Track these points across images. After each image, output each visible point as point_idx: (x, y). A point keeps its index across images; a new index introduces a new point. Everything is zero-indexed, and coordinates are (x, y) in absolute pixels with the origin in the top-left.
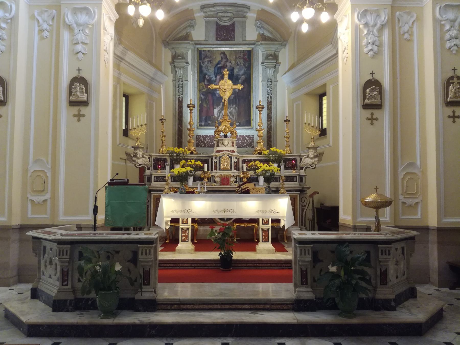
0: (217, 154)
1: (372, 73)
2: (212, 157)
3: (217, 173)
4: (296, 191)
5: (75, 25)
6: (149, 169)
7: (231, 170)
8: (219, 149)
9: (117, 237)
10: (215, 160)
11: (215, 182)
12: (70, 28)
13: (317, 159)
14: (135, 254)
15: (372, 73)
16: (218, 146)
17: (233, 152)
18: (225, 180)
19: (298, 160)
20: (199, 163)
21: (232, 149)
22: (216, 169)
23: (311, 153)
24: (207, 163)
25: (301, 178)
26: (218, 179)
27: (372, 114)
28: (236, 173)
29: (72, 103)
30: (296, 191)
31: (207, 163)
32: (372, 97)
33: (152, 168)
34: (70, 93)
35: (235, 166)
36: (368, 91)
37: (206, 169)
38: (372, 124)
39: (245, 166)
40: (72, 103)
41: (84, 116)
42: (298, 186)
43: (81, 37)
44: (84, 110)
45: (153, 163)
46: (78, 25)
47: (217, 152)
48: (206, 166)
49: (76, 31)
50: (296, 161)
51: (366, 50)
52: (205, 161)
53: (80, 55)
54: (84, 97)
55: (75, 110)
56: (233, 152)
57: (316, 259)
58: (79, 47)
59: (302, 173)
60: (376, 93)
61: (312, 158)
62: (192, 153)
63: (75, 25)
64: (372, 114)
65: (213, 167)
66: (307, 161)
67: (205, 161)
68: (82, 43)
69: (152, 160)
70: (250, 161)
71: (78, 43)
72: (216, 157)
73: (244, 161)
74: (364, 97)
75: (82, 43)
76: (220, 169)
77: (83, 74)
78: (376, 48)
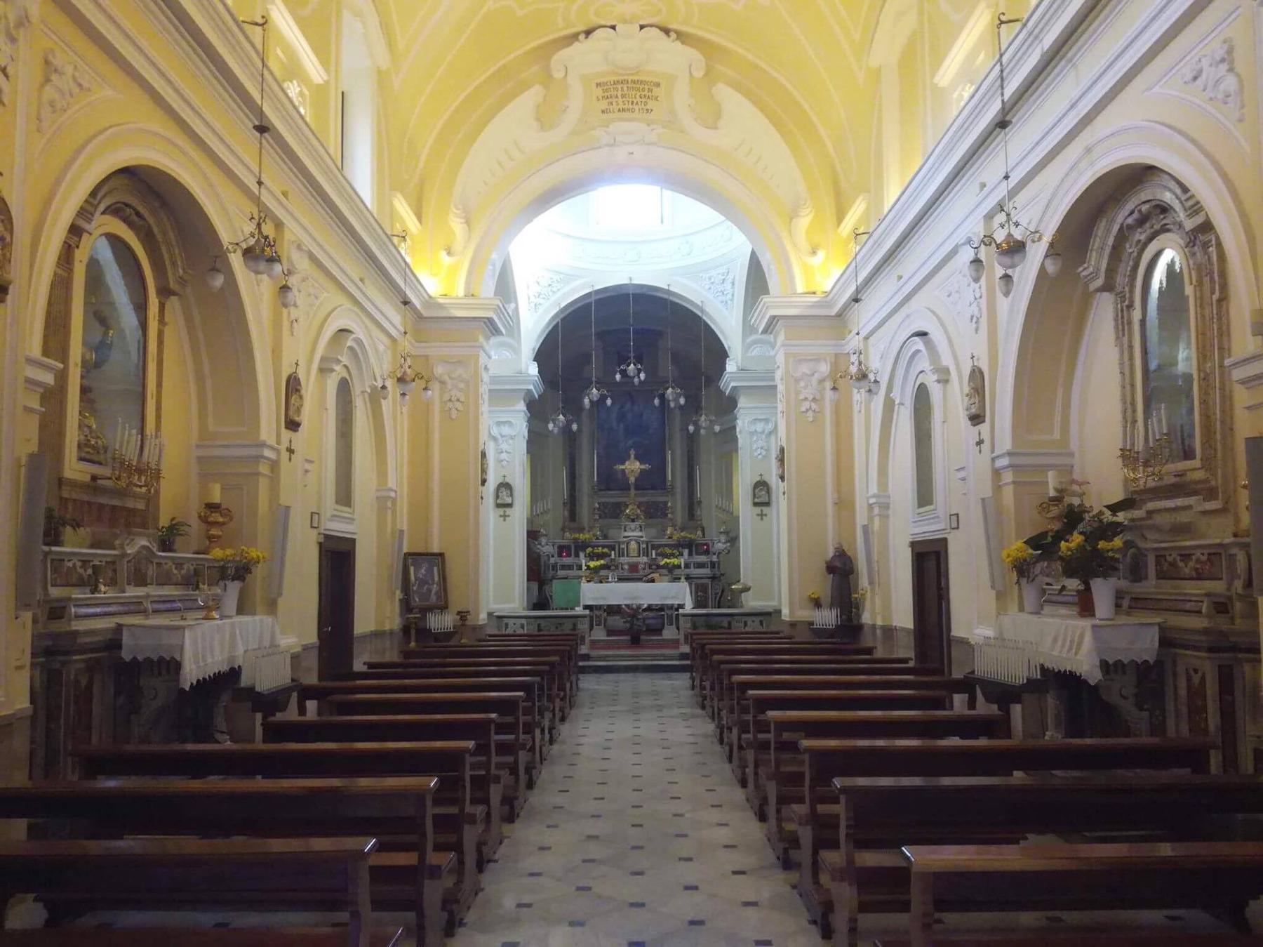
0: (625, 539)
1: (761, 475)
2: (619, 543)
3: (624, 560)
4: (709, 578)
5: (499, 437)
6: (553, 556)
7: (639, 556)
8: (626, 534)
9: (564, 613)
10: (622, 546)
11: (622, 569)
12: (495, 439)
13: (728, 544)
14: (575, 625)
15: (761, 475)
16: (625, 531)
17: (642, 537)
18: (634, 567)
19: (711, 545)
20: (606, 550)
21: (640, 534)
22: (623, 556)
23: (723, 538)
24: (614, 549)
25: (713, 565)
26: (626, 567)
27: (762, 511)
28: (645, 559)
29: (498, 506)
30: (709, 578)
31: (614, 549)
32: (760, 497)
33: (556, 556)
34: (497, 497)
35: (644, 553)
36: (757, 491)
37: (613, 557)
38: (762, 519)
39: (654, 552)
40: (498, 506)
41: (509, 516)
42: (709, 572)
43: (504, 446)
44: (508, 511)
45: (556, 550)
46: (502, 436)
47: (625, 537)
48: (613, 552)
49: (501, 442)
50: (708, 546)
51: (756, 454)
52: (612, 548)
53: (504, 463)
54: (509, 500)
55: (501, 511)
56: (642, 537)
57: (695, 627)
58: (504, 456)
59: (715, 558)
60: (763, 493)
61: (724, 543)
62: (597, 539)
63: (499, 437)
64: (762, 511)
65: (621, 554)
66: (720, 546)
67: (612, 548)
68: (506, 452)
69: (556, 547)
70: (660, 546)
71: (502, 452)
72: (623, 543)
73: (654, 547)
74: (754, 496)
75: (506, 452)
76: (627, 556)
77: (508, 480)
78: (764, 453)
